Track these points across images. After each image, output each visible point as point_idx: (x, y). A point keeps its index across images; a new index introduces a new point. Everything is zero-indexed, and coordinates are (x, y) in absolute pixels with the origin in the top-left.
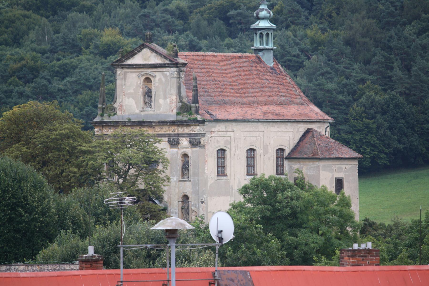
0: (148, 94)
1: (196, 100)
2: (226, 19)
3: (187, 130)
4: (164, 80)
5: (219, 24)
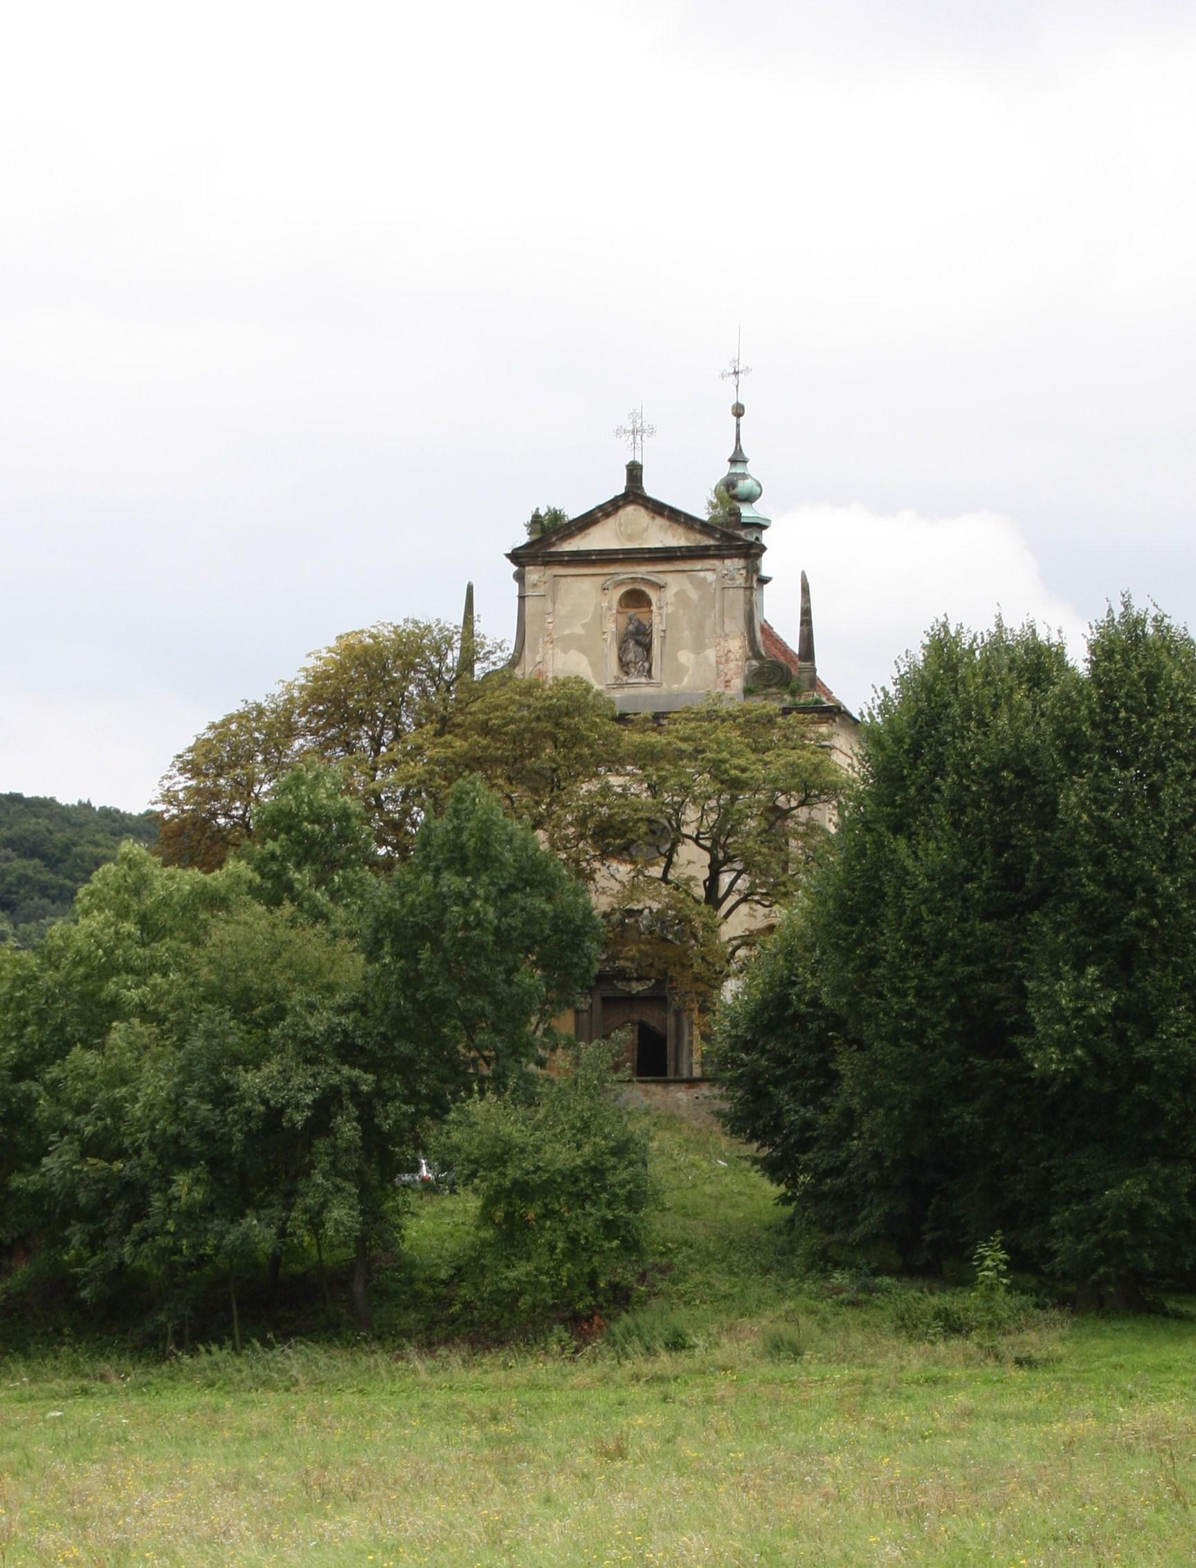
4: (694, 595)
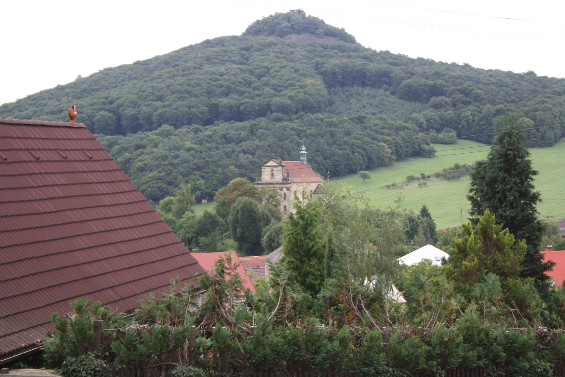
0: (272, 175)
1: (288, 177)
2: (226, 138)
3: (285, 186)
5: (223, 140)
